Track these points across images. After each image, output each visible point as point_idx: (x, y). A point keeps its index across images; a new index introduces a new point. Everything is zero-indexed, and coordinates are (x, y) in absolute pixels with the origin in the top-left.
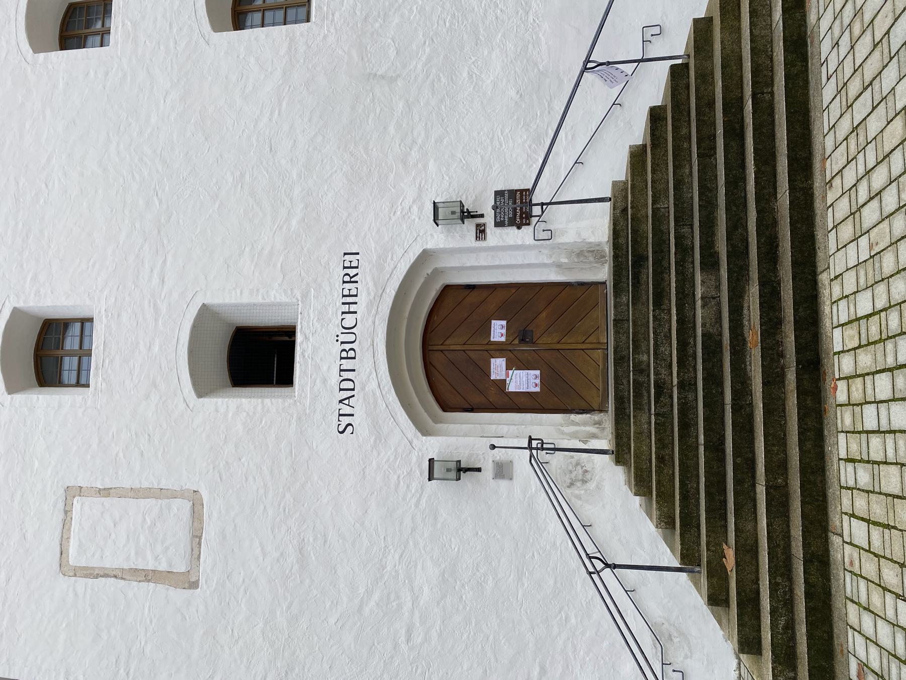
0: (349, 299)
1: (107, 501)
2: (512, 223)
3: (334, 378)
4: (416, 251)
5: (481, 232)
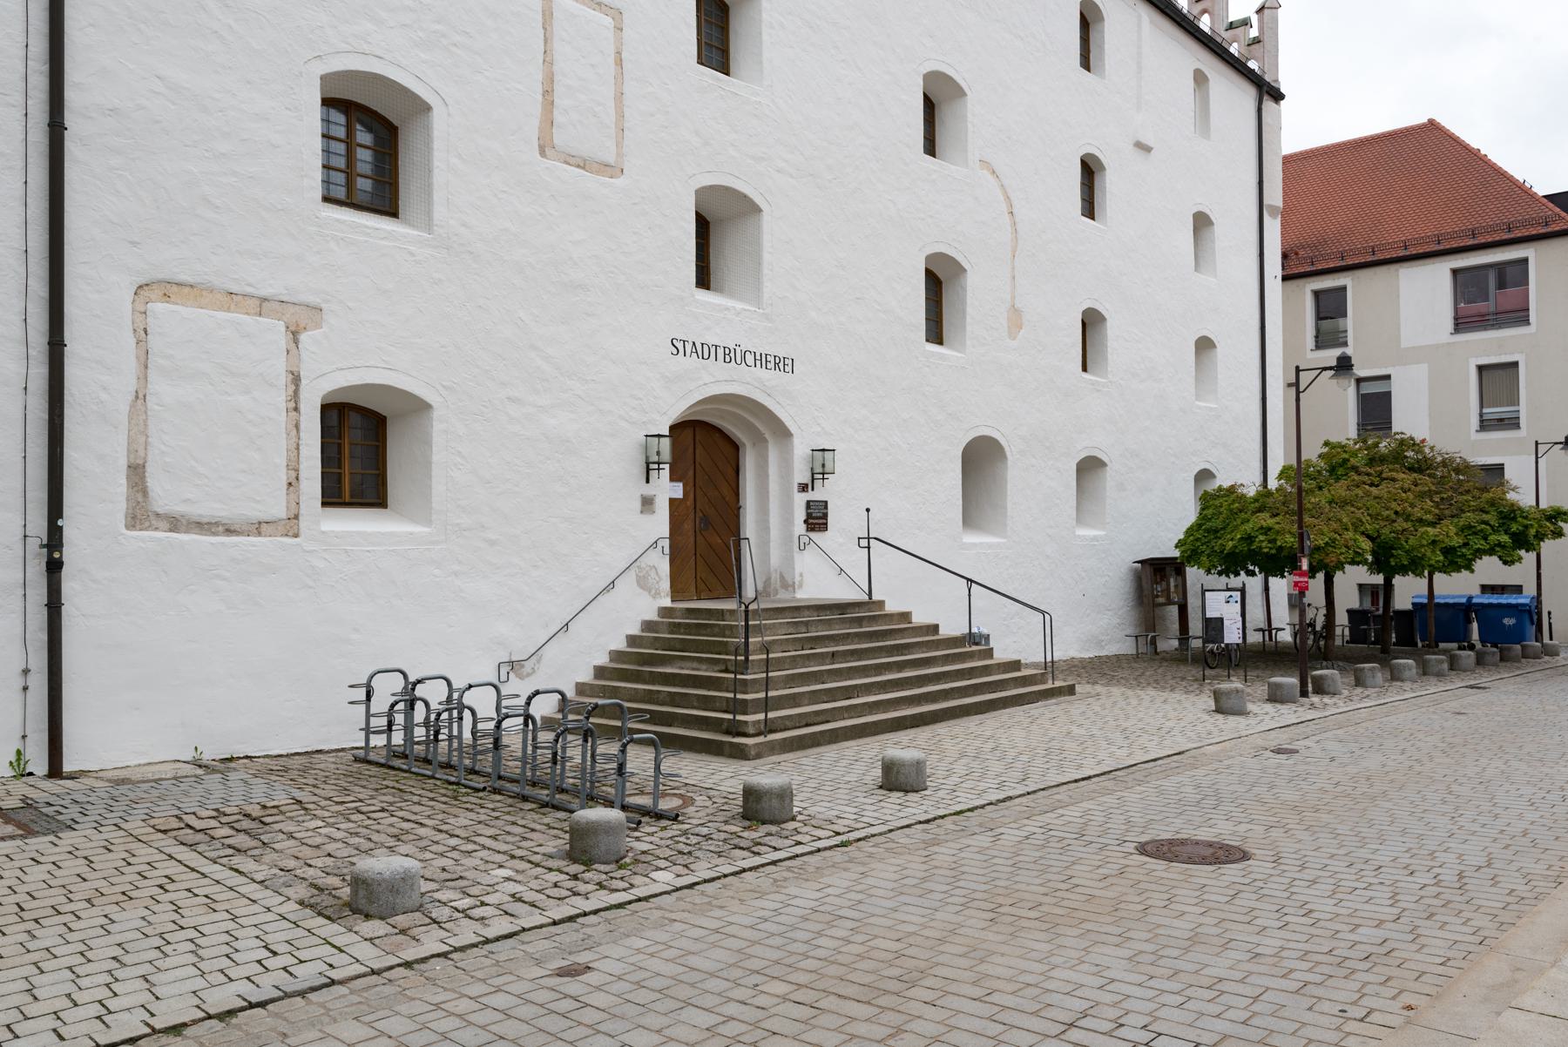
0: (762, 360)
1: (611, 60)
2: (809, 516)
3: (711, 341)
4: (792, 429)
5: (803, 488)
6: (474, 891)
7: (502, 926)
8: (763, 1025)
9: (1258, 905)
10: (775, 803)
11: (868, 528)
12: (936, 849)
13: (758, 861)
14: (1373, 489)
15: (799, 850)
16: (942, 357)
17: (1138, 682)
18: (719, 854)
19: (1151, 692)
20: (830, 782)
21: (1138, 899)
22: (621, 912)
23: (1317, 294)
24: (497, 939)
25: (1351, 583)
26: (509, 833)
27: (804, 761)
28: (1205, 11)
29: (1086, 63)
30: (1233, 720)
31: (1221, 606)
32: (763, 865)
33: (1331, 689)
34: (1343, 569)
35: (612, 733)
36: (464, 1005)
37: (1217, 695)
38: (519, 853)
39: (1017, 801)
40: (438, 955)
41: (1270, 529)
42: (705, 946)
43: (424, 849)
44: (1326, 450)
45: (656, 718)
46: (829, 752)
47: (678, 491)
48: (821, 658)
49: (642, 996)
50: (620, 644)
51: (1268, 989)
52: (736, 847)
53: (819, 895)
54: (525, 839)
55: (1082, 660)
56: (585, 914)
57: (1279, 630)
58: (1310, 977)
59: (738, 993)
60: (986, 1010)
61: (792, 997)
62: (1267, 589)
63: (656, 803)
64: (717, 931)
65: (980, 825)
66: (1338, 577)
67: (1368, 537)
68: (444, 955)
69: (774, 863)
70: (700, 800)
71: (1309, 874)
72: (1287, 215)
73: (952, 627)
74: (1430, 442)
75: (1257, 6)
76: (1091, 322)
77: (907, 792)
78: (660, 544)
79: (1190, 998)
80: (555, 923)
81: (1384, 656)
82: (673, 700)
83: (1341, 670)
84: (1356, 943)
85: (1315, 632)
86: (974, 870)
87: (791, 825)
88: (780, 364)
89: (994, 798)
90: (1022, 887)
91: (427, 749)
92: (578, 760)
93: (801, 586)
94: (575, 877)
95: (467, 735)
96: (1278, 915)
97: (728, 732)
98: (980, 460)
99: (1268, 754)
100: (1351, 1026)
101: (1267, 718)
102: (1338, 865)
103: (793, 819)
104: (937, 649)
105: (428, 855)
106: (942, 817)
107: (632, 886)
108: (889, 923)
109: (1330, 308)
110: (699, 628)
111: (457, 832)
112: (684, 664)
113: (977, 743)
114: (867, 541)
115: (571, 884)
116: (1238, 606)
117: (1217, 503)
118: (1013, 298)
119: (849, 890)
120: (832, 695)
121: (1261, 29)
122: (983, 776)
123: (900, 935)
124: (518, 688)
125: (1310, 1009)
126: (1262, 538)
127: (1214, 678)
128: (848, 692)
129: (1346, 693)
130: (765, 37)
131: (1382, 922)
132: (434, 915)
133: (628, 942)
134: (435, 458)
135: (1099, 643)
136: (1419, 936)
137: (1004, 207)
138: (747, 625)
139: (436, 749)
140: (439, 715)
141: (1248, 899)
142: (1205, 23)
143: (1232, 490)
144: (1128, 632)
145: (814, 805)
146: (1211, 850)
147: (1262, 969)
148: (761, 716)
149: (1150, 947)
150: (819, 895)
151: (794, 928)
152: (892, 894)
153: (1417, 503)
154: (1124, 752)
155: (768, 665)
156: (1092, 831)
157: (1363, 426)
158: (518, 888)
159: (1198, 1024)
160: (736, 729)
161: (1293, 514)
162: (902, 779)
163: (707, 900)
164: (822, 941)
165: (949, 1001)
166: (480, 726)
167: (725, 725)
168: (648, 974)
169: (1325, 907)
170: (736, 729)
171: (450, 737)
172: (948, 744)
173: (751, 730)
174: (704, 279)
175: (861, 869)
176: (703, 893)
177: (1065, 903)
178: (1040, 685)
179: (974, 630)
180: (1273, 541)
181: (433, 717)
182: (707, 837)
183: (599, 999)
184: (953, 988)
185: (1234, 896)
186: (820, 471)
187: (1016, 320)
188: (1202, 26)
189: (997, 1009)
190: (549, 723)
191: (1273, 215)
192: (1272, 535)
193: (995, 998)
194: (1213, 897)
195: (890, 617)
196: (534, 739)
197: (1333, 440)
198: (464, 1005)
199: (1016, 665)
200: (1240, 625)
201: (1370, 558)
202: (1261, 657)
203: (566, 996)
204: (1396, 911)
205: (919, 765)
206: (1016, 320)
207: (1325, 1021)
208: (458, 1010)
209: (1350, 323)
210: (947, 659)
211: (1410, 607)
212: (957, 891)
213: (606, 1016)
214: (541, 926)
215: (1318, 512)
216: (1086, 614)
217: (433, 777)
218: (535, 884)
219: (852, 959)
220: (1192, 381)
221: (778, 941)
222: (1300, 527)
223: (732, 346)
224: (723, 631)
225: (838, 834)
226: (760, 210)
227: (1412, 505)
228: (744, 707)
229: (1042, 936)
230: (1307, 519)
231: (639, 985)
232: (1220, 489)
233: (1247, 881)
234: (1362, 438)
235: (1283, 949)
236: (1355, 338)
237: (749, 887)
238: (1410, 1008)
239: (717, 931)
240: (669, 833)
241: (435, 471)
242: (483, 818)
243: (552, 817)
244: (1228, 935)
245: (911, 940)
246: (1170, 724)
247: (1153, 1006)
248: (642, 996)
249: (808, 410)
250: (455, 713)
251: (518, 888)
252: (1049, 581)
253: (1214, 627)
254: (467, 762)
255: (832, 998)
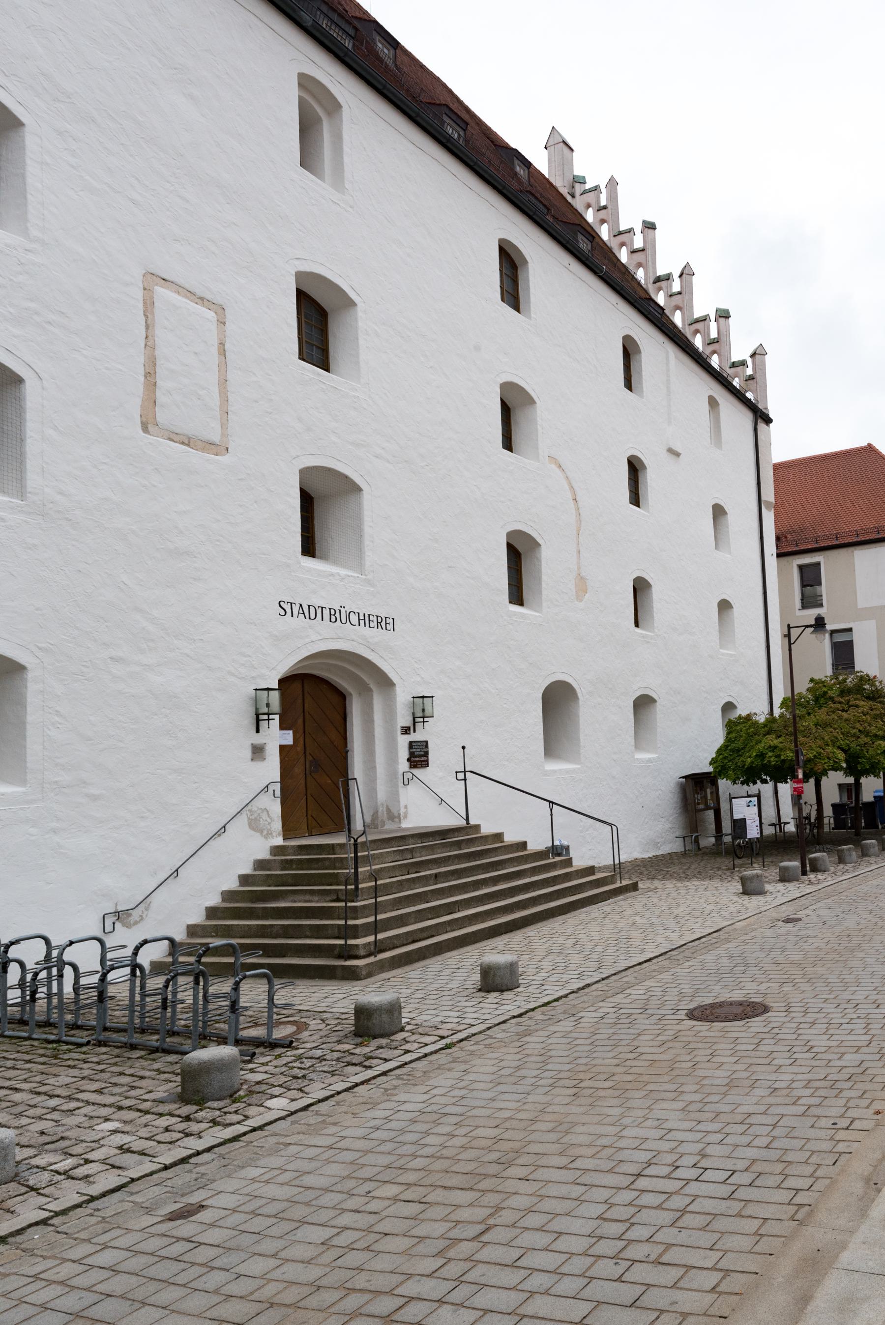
0: (365, 620)
1: (215, 350)
2: (412, 755)
3: (318, 603)
5: (406, 730)
6: (78, 1150)
7: (112, 1179)
8: (376, 1229)
9: (776, 1048)
10: (385, 1018)
11: (464, 765)
12: (528, 1039)
13: (370, 1073)
14: (844, 713)
15: (407, 1058)
16: (523, 616)
17: (685, 875)
18: (333, 1073)
19: (696, 882)
20: (433, 992)
21: (688, 1058)
22: (237, 1145)
23: (801, 568)
24: (104, 1195)
25: (833, 783)
26: (116, 1084)
27: (412, 974)
28: (714, 352)
29: (628, 385)
30: (756, 900)
31: (744, 809)
32: (374, 1078)
33: (823, 868)
34: (826, 775)
35: (223, 971)
36: (66, 1270)
37: (744, 881)
38: (127, 1103)
39: (594, 987)
40: (37, 1224)
41: (775, 747)
42: (319, 1164)
43: (20, 1115)
44: (812, 685)
45: (269, 951)
46: (434, 964)
47: (288, 738)
48: (425, 880)
49: (258, 1224)
50: (232, 884)
51: (783, 1115)
52: (350, 1064)
53: (427, 1097)
54: (133, 1088)
55: (643, 860)
56: (198, 1153)
57: (786, 823)
58: (813, 1101)
59: (351, 1204)
60: (569, 1175)
61: (402, 1197)
62: (776, 792)
63: (270, 1033)
64: (331, 1147)
65: (564, 1013)
66: (824, 781)
67: (842, 750)
68: (44, 1222)
69: (384, 1073)
70: (314, 1024)
71: (810, 1018)
72: (778, 508)
73: (537, 843)
74: (879, 678)
75: (751, 352)
76: (640, 588)
77: (502, 991)
78: (271, 788)
79: (728, 1134)
80: (166, 1168)
81: (856, 839)
82: (286, 932)
83: (829, 852)
84: (843, 1067)
85: (810, 823)
86: (560, 1053)
87: (400, 1036)
88: (383, 623)
89: (575, 987)
90: (599, 1061)
91: (23, 1011)
92: (190, 1001)
93: (405, 817)
94: (188, 1118)
95: (68, 989)
96: (789, 1054)
97: (340, 957)
98: (557, 700)
99: (781, 924)
100: (841, 1135)
101: (780, 894)
102: (830, 1007)
103: (402, 1030)
104: (526, 863)
105: (24, 1121)
106: (533, 1010)
107: (247, 1117)
108: (488, 1112)
109: (810, 578)
110: (310, 863)
111: (58, 1092)
112: (297, 897)
113: (561, 941)
114: (463, 775)
115: (183, 1126)
116: (756, 808)
117: (738, 728)
118: (579, 568)
119: (453, 1088)
120: (435, 912)
121: (754, 369)
122: (565, 970)
123: (497, 1122)
124: (124, 938)
125: (812, 1126)
126: (770, 754)
127: (741, 866)
128: (450, 908)
129: (832, 869)
130: (361, 342)
131: (859, 1048)
132: (31, 1183)
133: (243, 1173)
134: (30, 718)
135: (656, 845)
136: (812, 1047)
137: (569, 495)
138: (356, 857)
139: (32, 1009)
140: (36, 974)
141: (767, 1046)
142: (715, 362)
143: (748, 717)
144: (677, 834)
145: (420, 1014)
146: (741, 1008)
147: (779, 1100)
148: (371, 938)
149: (698, 1097)
150: (427, 1097)
151: (403, 1131)
152: (491, 1085)
153: (873, 723)
154: (675, 935)
155: (376, 891)
156: (653, 1004)
157: (835, 666)
158: (126, 1139)
159: (734, 1155)
160: (348, 953)
161: (791, 735)
162: (498, 980)
163: (320, 1119)
164: (430, 1140)
165: (542, 1174)
166: (83, 981)
167: (336, 952)
168: (264, 1201)
169: (821, 1042)
170: (348, 953)
171: (49, 995)
172: (537, 944)
173: (362, 952)
174: (309, 548)
175: (463, 1067)
176: (317, 1113)
177: (633, 1070)
178: (611, 884)
179: (557, 843)
180: (778, 756)
181: (29, 977)
182: (321, 1059)
183: (214, 1236)
184: (544, 1161)
185: (758, 1044)
186: (421, 712)
187: (582, 585)
188: (713, 364)
189: (579, 1173)
190: (158, 968)
191: (768, 508)
192: (777, 752)
193: (578, 1164)
194: (743, 1047)
195: (485, 839)
196: (143, 987)
197: (816, 677)
198: (66, 1270)
199: (591, 870)
200: (758, 823)
201: (844, 765)
202: (774, 846)
203: (179, 1239)
204: (868, 1037)
205: (512, 967)
206: (582, 585)
207: (822, 1134)
208: (210, 1286)
209: (824, 589)
210: (535, 871)
211: (872, 799)
212: (546, 1074)
213: (221, 1250)
214: (151, 1174)
215: (807, 733)
216: (647, 827)
217: (29, 1038)
218: (144, 1132)
219: (455, 1151)
220: (716, 634)
221: (388, 1147)
222: (796, 746)
223: (337, 608)
224: (333, 864)
225: (442, 1038)
226: (360, 490)
227: (870, 725)
228: (355, 932)
229: (616, 1102)
230: (801, 739)
231: (255, 1214)
232: (740, 717)
233: (766, 1030)
234: (835, 675)
235: (793, 1081)
236: (828, 601)
237: (361, 1100)
238: (878, 1113)
239: (331, 1147)
240: (284, 1060)
241: (30, 731)
242: (86, 1073)
243: (163, 1062)
244: (754, 1077)
245: (507, 1125)
246: (710, 907)
247: (701, 1146)
248: (258, 1224)
249: (408, 663)
250: (54, 971)
251: (126, 1139)
252: (609, 799)
253: (740, 825)
254: (69, 1017)
255: (439, 1191)
